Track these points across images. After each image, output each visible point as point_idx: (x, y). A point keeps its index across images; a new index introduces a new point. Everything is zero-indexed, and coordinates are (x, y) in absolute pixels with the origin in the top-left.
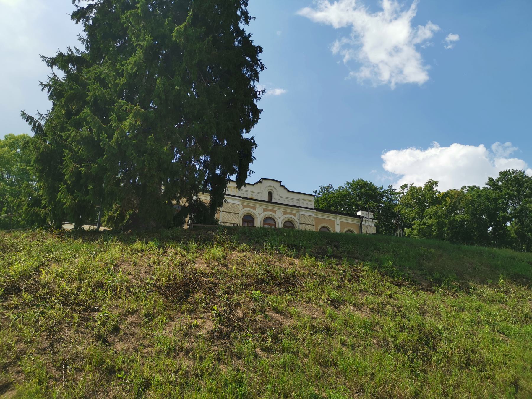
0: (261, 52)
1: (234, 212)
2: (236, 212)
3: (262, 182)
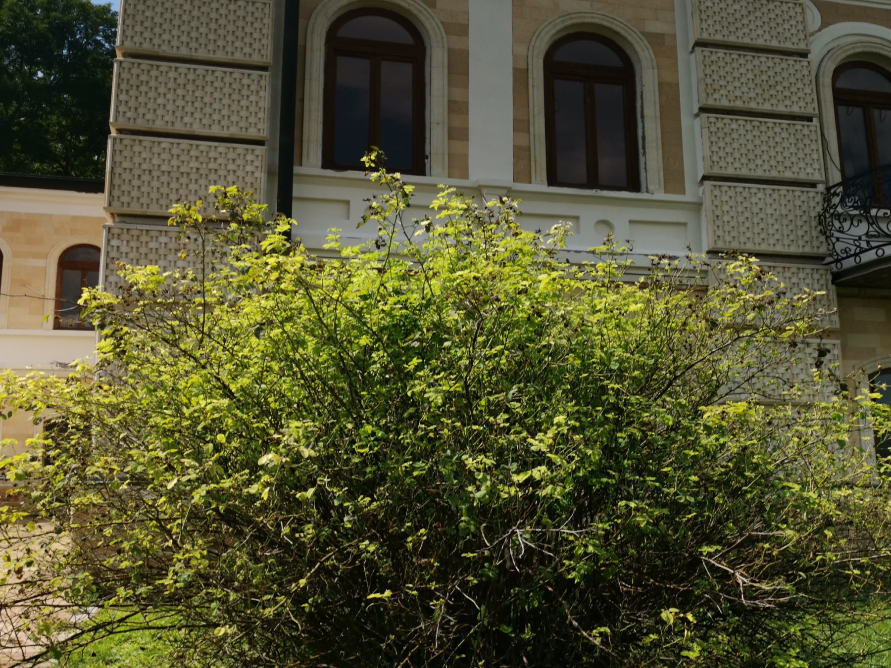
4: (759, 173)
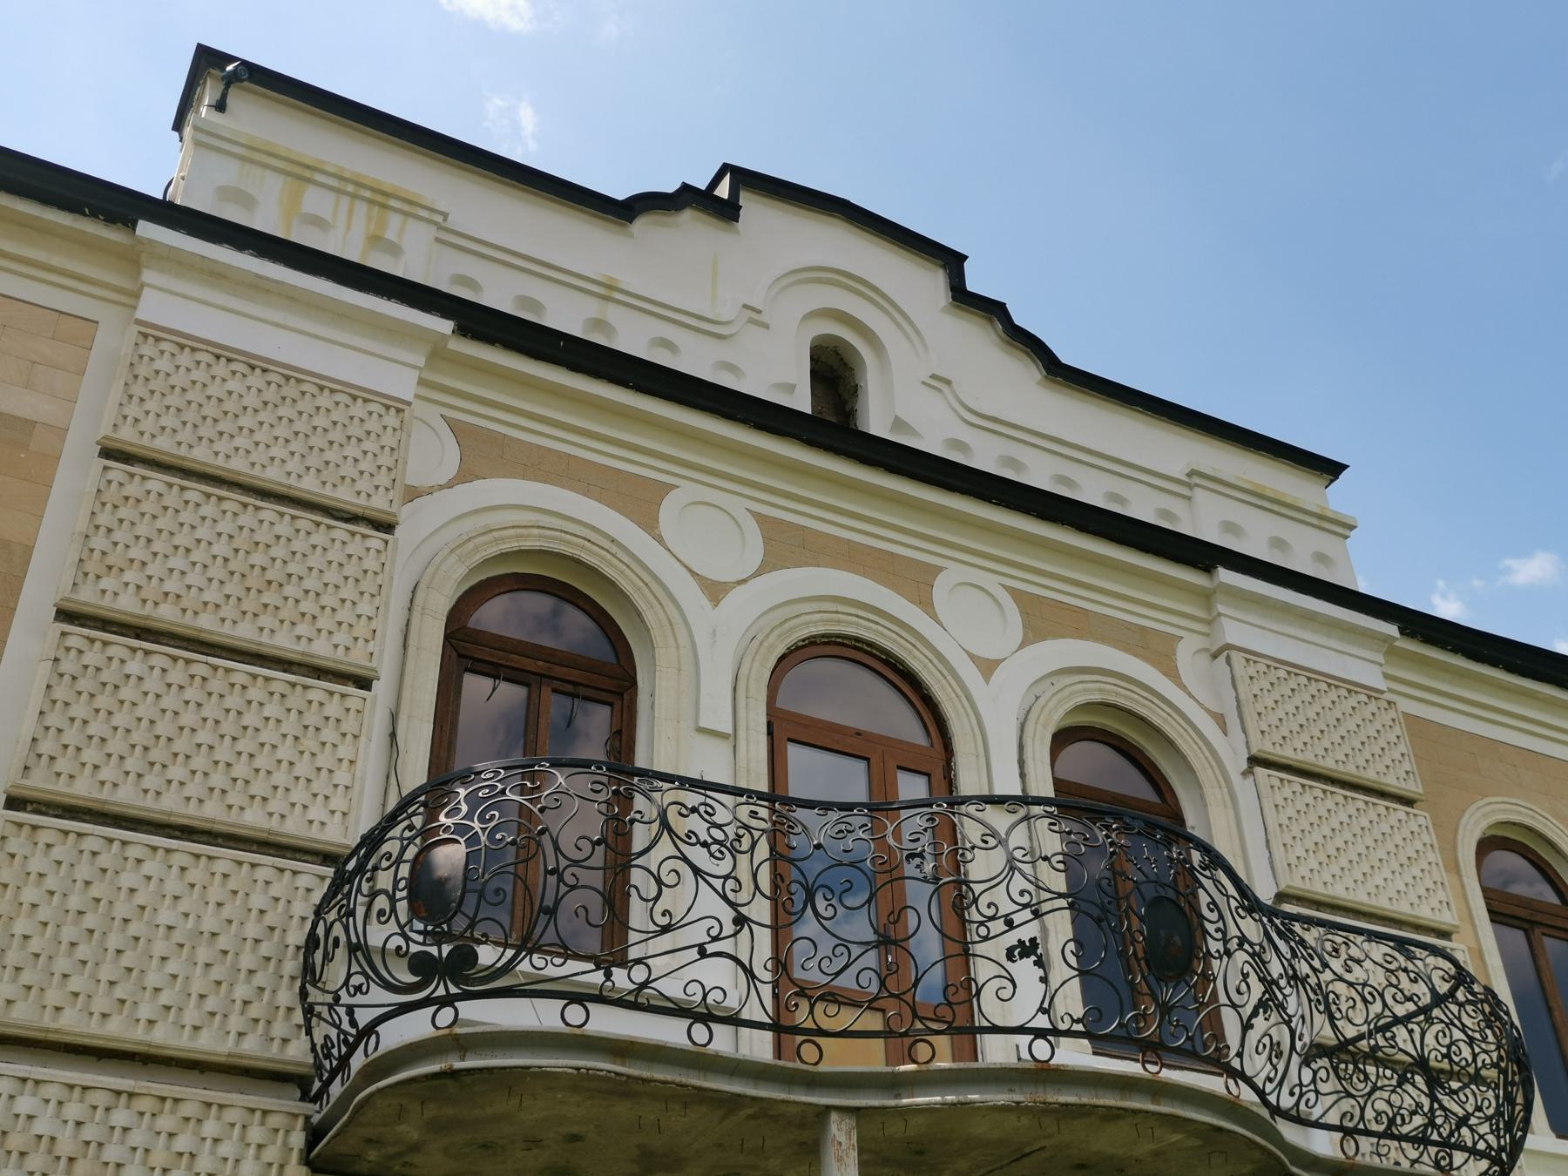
0: (1041, 978)
1: (309, 486)
2: (344, 496)
3: (728, 211)
4: (171, 805)
